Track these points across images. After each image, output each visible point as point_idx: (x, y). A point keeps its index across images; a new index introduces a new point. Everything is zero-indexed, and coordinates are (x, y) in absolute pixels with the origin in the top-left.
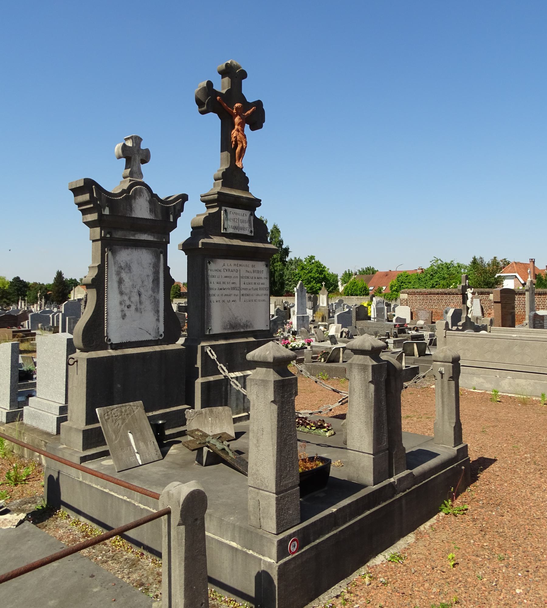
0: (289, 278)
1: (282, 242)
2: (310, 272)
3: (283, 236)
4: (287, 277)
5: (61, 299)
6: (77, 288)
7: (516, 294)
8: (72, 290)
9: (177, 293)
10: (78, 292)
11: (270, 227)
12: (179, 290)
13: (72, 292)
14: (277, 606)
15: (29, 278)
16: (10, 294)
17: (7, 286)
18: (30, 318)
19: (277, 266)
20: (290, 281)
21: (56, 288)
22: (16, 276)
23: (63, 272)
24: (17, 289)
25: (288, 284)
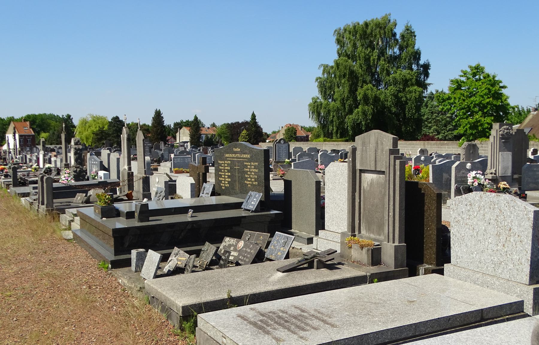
0: (428, 119)
1: (420, 55)
2: (472, 95)
3: (419, 44)
4: (426, 117)
6: (182, 130)
7: (198, 180)
9: (292, 136)
11: (399, 31)
12: (295, 133)
13: (178, 134)
16: (109, 135)
17: (106, 127)
19: (411, 92)
20: (430, 123)
22: (115, 116)
24: (116, 130)
25: (427, 126)
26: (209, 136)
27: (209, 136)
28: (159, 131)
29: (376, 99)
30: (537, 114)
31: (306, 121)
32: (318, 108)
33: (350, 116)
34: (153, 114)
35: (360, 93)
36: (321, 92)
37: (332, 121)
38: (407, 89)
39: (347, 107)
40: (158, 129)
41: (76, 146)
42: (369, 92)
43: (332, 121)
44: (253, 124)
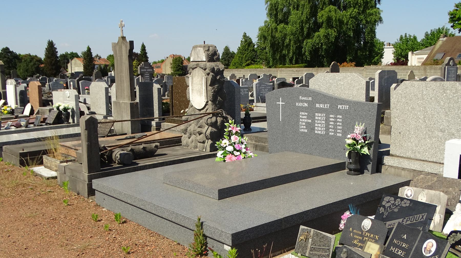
5: (54, 71)
6: (73, 61)
8: (68, 62)
9: (179, 66)
10: (75, 64)
12: (182, 63)
13: (69, 65)
14: (410, 257)
15: (20, 49)
18: (254, 89)
21: (49, 60)
22: (5, 47)
23: (54, 42)
26: (102, 66)
27: (102, 66)
28: (53, 62)
29: (341, 22)
30: (446, 40)
31: (106, 58)
32: (272, 32)
33: (309, 41)
34: (46, 46)
35: (322, 15)
36: (271, 14)
37: (288, 45)
38: (368, 11)
39: (305, 30)
40: (53, 60)
41: (213, 64)
42: (333, 13)
43: (288, 45)
44: (144, 54)
